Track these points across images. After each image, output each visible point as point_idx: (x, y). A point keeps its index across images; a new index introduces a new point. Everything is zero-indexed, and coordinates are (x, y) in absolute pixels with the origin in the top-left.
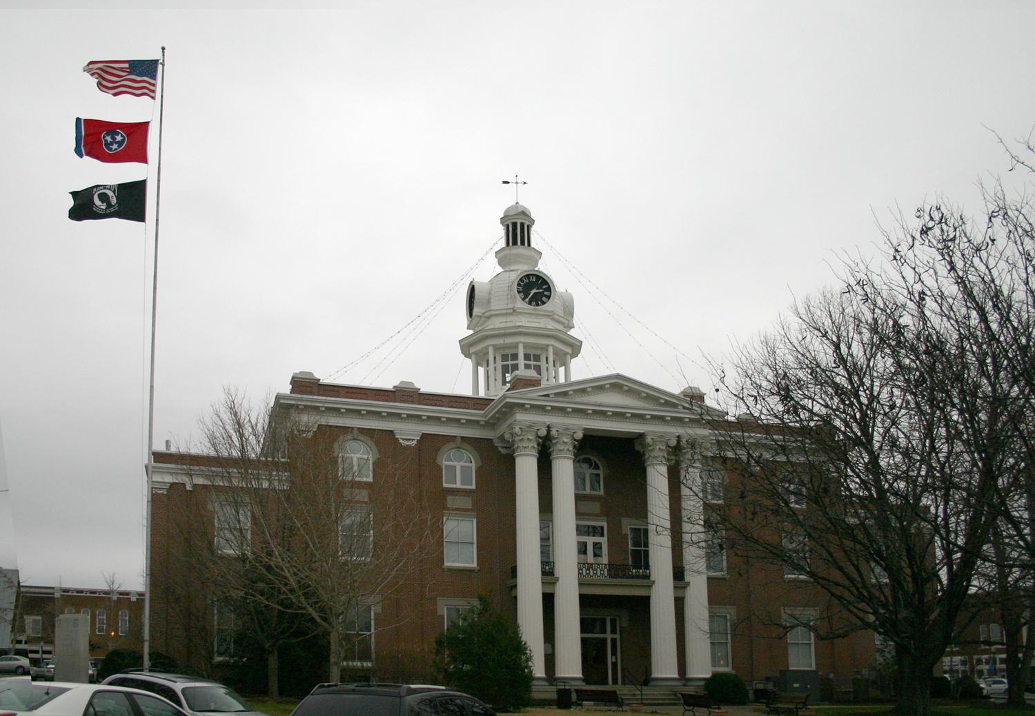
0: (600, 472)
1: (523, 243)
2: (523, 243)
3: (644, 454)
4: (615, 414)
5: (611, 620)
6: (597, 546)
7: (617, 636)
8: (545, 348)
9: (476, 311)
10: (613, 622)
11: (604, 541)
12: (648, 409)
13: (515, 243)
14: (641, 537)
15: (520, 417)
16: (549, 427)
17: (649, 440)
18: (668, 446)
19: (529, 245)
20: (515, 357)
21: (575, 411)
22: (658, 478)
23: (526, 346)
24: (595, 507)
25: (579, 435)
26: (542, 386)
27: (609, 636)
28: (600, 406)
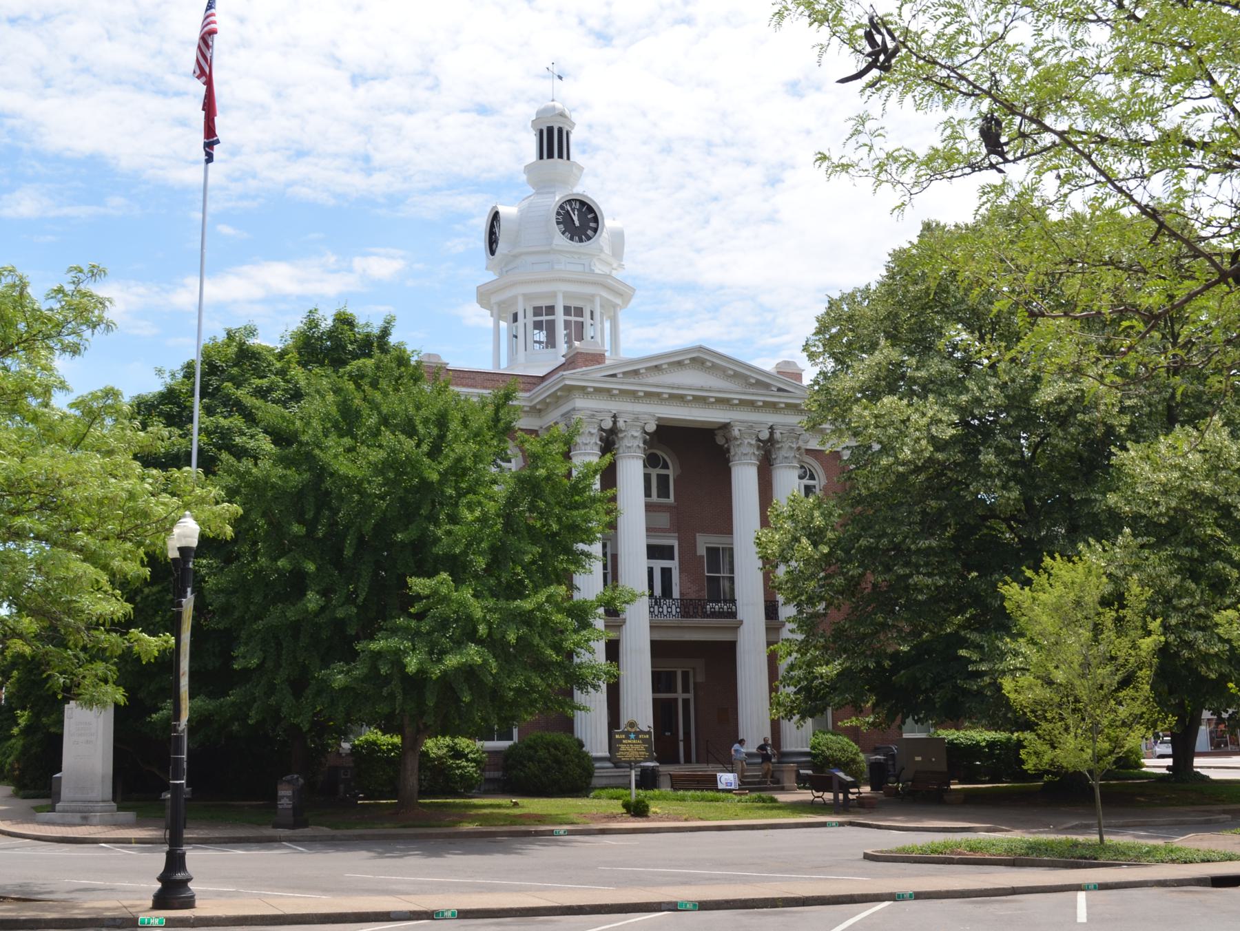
0: (670, 472)
1: (560, 156)
2: (560, 156)
3: (728, 450)
4: (696, 399)
5: (683, 673)
6: (666, 573)
7: (691, 696)
8: (591, 299)
9: (501, 248)
10: (685, 675)
11: (674, 564)
12: (734, 390)
13: (550, 156)
14: (721, 558)
15: (580, 402)
16: (615, 416)
17: (736, 433)
18: (759, 440)
19: (568, 158)
20: (551, 310)
21: (648, 395)
22: (745, 479)
23: (566, 295)
24: (664, 519)
25: (651, 427)
26: (607, 362)
27: (680, 696)
28: (678, 388)
